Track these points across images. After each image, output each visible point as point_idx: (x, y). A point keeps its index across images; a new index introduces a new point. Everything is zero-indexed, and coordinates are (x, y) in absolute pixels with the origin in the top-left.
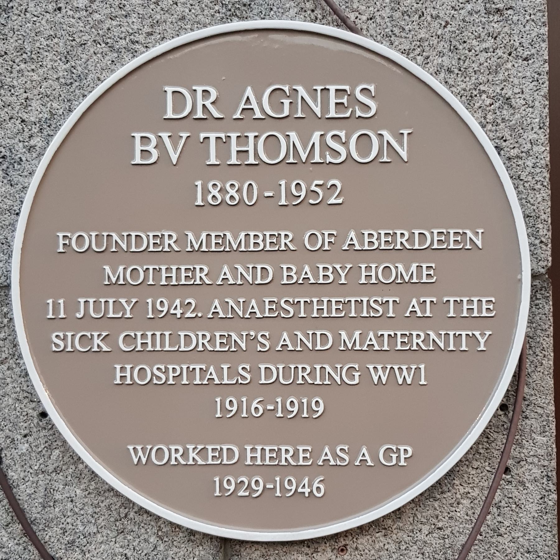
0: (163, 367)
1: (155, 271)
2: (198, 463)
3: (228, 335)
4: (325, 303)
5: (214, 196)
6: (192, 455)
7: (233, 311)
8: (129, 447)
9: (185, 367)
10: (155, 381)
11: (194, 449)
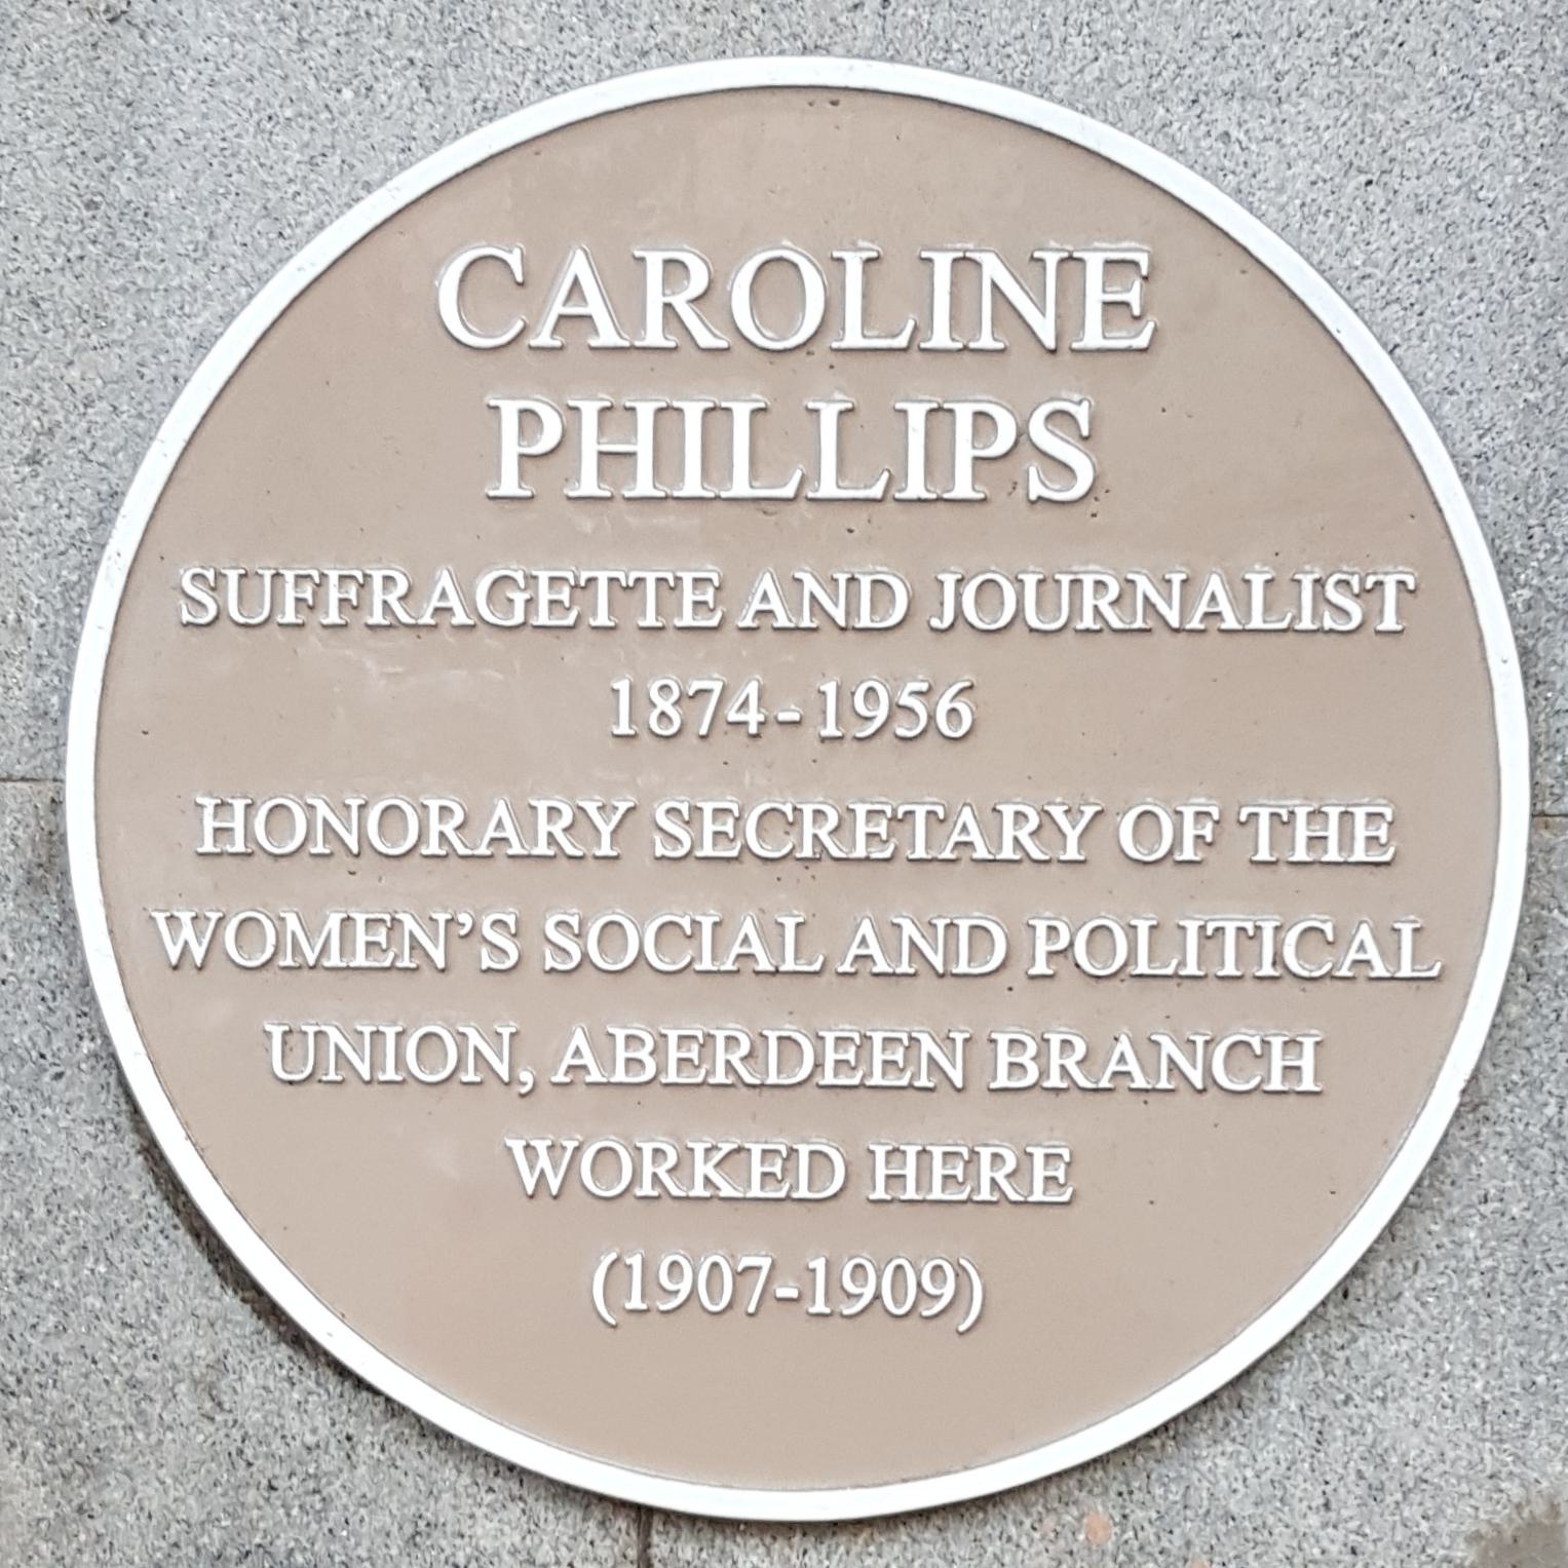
1: (664, 586)
2: (722, 1194)
3: (911, 1039)
5: (663, 714)
6: (702, 1168)
8: (510, 1143)
11: (707, 1151)
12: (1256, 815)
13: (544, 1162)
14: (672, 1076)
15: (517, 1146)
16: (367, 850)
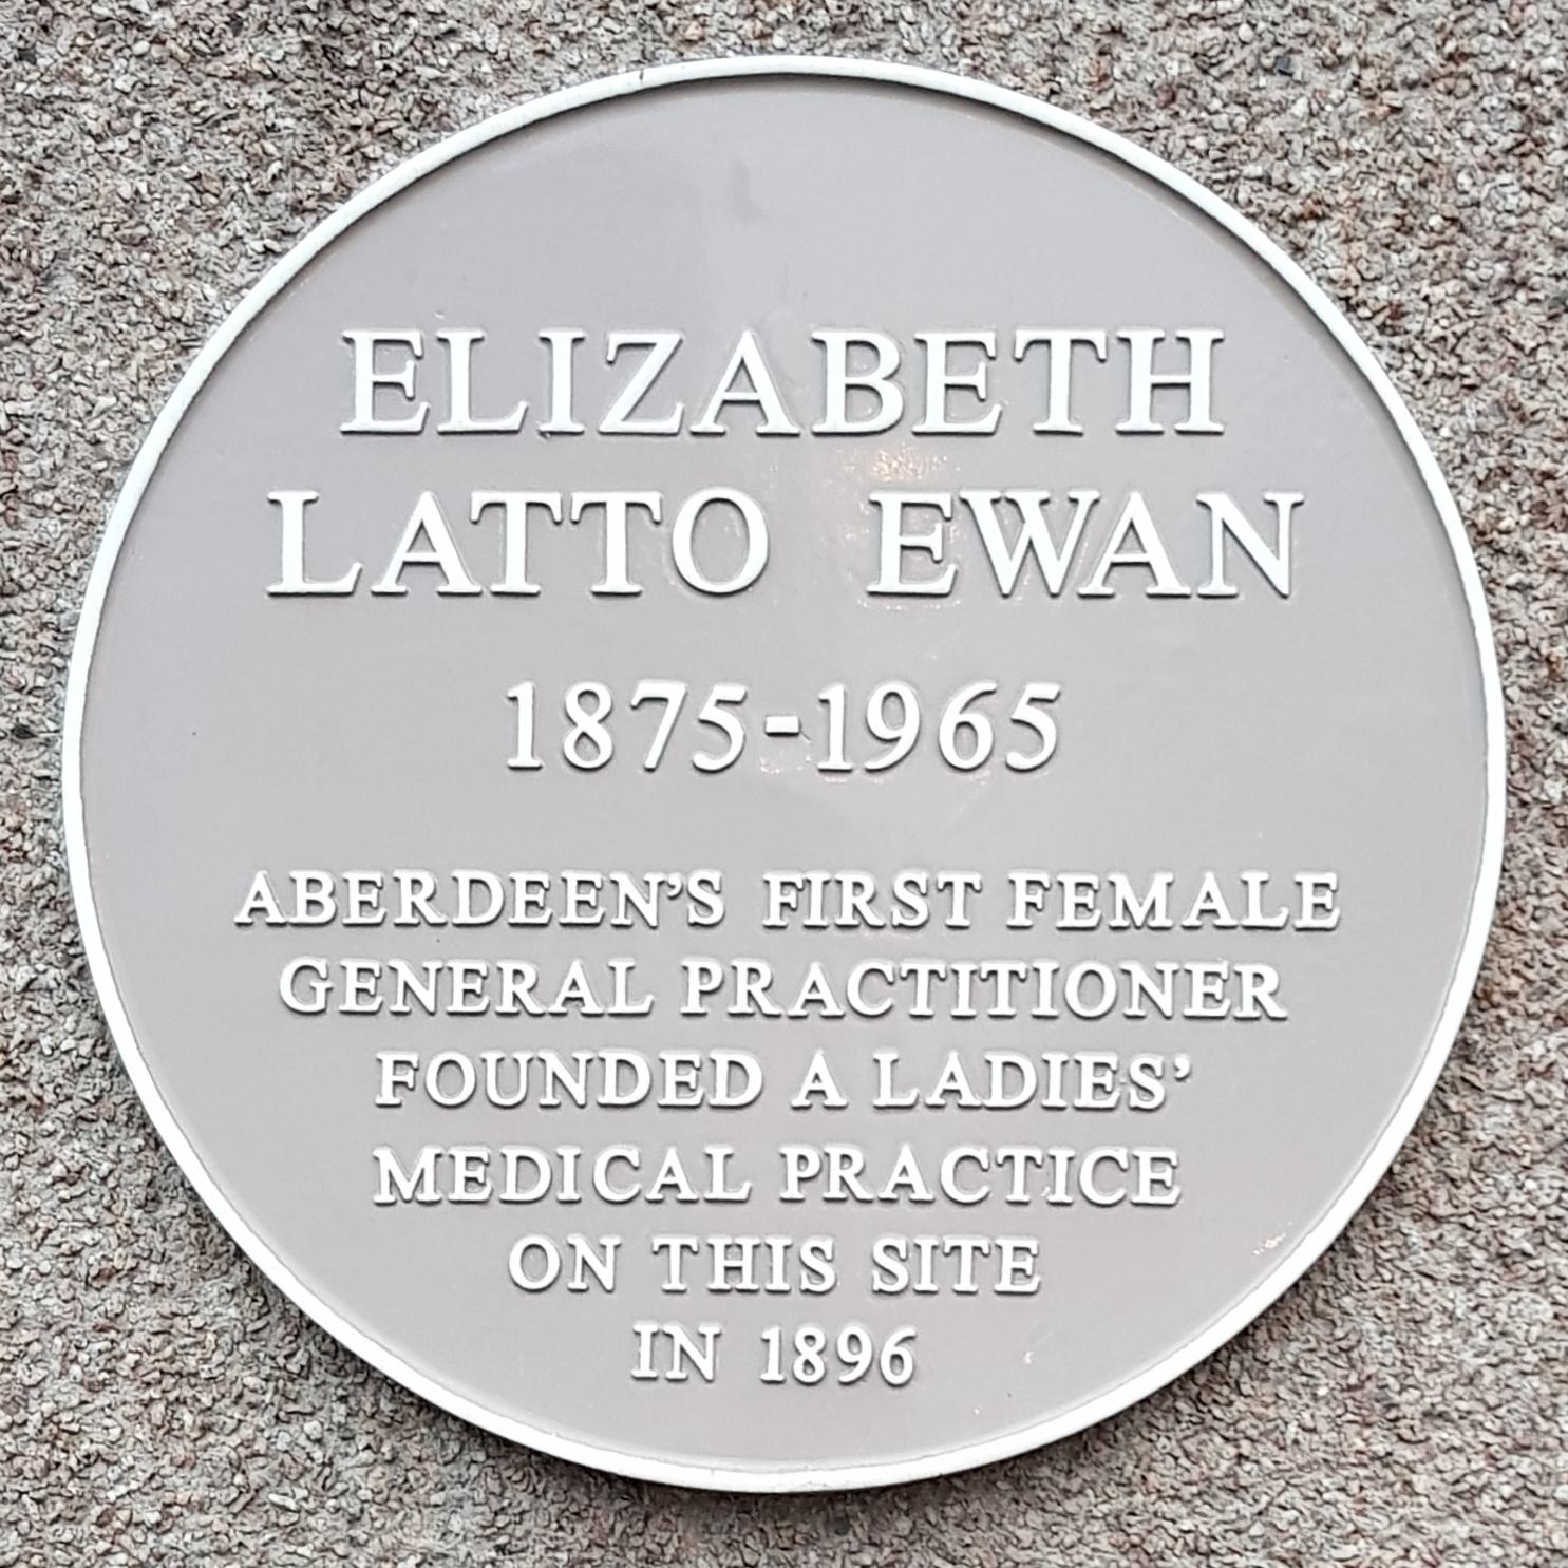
4: (748, 1251)
5: (584, 735)
13: (1035, 527)
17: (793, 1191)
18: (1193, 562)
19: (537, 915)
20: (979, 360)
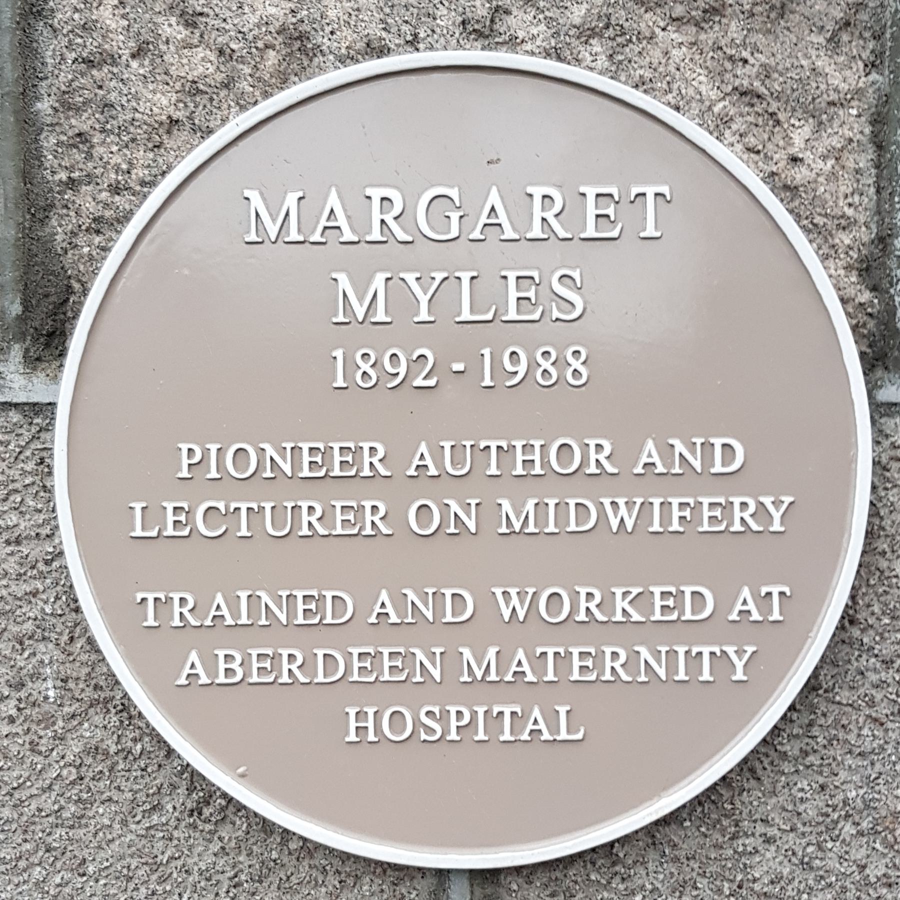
0: (436, 710)
4: (537, 449)
6: (621, 604)
7: (416, 612)
9: (481, 711)
10: (423, 736)
12: (546, 653)
13: (515, 601)
14: (255, 679)
15: (498, 591)
16: (444, 475)
17: (185, 473)
18: (669, 464)
19: (366, 676)
20: (531, 285)
